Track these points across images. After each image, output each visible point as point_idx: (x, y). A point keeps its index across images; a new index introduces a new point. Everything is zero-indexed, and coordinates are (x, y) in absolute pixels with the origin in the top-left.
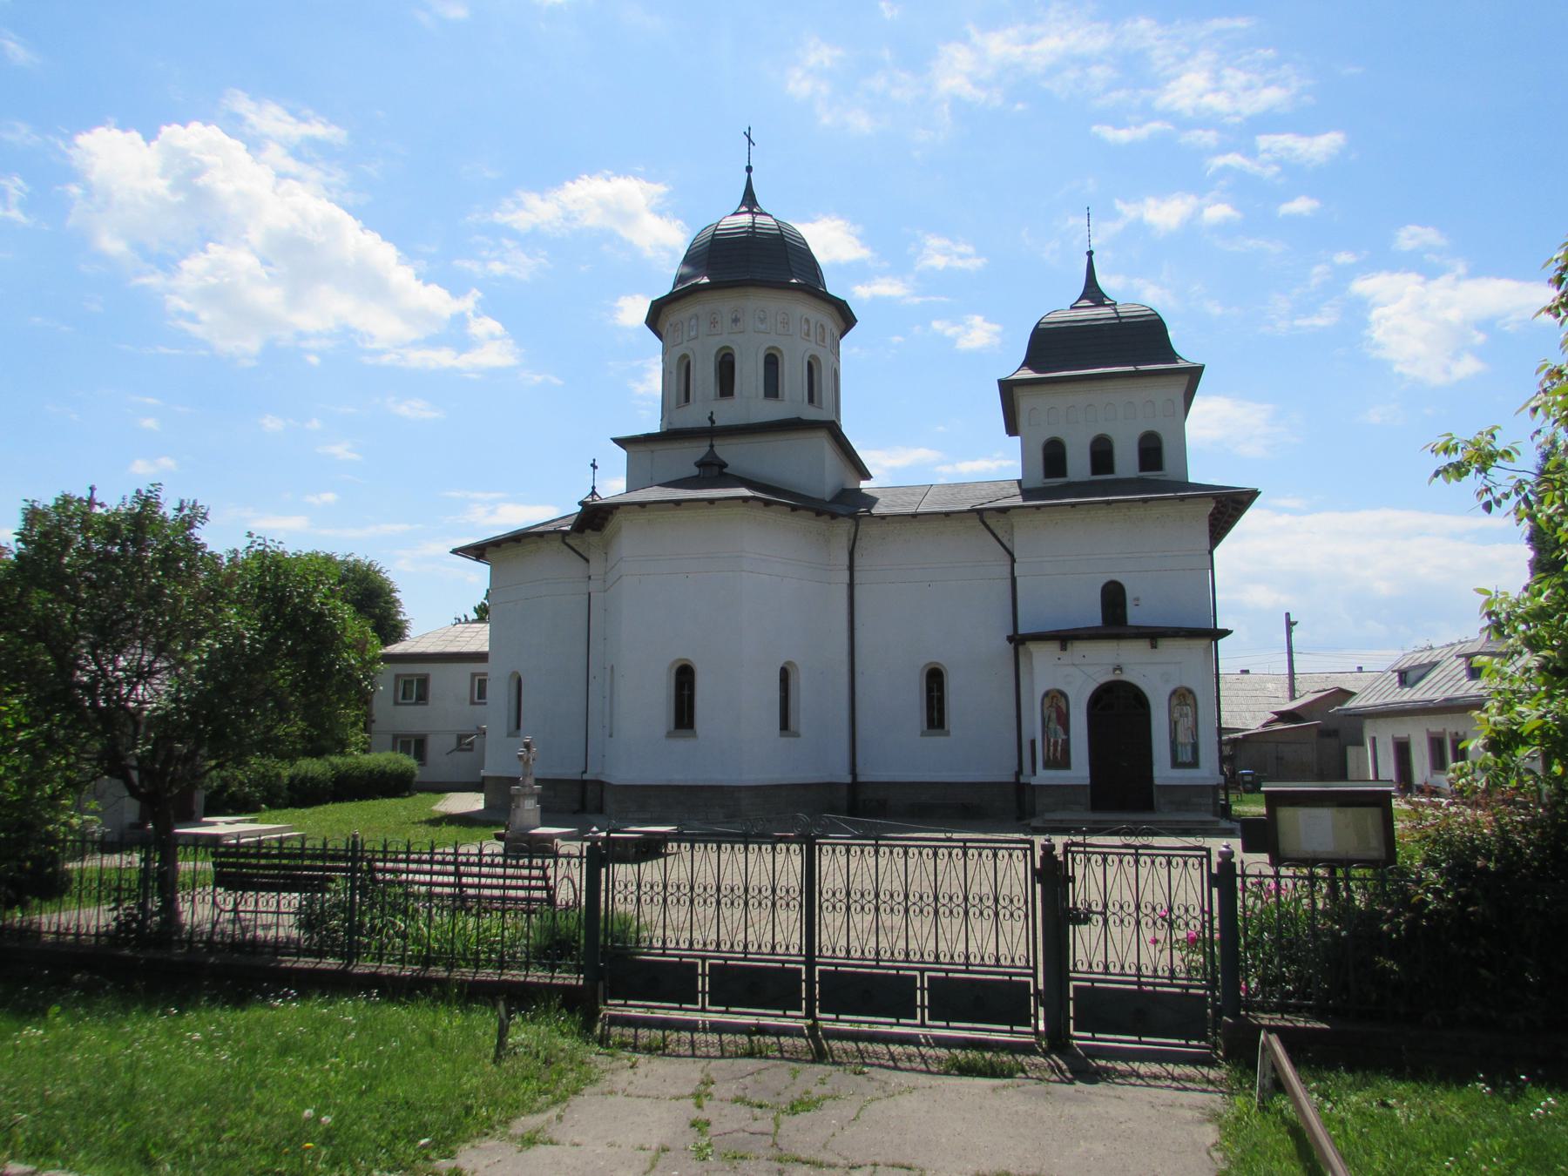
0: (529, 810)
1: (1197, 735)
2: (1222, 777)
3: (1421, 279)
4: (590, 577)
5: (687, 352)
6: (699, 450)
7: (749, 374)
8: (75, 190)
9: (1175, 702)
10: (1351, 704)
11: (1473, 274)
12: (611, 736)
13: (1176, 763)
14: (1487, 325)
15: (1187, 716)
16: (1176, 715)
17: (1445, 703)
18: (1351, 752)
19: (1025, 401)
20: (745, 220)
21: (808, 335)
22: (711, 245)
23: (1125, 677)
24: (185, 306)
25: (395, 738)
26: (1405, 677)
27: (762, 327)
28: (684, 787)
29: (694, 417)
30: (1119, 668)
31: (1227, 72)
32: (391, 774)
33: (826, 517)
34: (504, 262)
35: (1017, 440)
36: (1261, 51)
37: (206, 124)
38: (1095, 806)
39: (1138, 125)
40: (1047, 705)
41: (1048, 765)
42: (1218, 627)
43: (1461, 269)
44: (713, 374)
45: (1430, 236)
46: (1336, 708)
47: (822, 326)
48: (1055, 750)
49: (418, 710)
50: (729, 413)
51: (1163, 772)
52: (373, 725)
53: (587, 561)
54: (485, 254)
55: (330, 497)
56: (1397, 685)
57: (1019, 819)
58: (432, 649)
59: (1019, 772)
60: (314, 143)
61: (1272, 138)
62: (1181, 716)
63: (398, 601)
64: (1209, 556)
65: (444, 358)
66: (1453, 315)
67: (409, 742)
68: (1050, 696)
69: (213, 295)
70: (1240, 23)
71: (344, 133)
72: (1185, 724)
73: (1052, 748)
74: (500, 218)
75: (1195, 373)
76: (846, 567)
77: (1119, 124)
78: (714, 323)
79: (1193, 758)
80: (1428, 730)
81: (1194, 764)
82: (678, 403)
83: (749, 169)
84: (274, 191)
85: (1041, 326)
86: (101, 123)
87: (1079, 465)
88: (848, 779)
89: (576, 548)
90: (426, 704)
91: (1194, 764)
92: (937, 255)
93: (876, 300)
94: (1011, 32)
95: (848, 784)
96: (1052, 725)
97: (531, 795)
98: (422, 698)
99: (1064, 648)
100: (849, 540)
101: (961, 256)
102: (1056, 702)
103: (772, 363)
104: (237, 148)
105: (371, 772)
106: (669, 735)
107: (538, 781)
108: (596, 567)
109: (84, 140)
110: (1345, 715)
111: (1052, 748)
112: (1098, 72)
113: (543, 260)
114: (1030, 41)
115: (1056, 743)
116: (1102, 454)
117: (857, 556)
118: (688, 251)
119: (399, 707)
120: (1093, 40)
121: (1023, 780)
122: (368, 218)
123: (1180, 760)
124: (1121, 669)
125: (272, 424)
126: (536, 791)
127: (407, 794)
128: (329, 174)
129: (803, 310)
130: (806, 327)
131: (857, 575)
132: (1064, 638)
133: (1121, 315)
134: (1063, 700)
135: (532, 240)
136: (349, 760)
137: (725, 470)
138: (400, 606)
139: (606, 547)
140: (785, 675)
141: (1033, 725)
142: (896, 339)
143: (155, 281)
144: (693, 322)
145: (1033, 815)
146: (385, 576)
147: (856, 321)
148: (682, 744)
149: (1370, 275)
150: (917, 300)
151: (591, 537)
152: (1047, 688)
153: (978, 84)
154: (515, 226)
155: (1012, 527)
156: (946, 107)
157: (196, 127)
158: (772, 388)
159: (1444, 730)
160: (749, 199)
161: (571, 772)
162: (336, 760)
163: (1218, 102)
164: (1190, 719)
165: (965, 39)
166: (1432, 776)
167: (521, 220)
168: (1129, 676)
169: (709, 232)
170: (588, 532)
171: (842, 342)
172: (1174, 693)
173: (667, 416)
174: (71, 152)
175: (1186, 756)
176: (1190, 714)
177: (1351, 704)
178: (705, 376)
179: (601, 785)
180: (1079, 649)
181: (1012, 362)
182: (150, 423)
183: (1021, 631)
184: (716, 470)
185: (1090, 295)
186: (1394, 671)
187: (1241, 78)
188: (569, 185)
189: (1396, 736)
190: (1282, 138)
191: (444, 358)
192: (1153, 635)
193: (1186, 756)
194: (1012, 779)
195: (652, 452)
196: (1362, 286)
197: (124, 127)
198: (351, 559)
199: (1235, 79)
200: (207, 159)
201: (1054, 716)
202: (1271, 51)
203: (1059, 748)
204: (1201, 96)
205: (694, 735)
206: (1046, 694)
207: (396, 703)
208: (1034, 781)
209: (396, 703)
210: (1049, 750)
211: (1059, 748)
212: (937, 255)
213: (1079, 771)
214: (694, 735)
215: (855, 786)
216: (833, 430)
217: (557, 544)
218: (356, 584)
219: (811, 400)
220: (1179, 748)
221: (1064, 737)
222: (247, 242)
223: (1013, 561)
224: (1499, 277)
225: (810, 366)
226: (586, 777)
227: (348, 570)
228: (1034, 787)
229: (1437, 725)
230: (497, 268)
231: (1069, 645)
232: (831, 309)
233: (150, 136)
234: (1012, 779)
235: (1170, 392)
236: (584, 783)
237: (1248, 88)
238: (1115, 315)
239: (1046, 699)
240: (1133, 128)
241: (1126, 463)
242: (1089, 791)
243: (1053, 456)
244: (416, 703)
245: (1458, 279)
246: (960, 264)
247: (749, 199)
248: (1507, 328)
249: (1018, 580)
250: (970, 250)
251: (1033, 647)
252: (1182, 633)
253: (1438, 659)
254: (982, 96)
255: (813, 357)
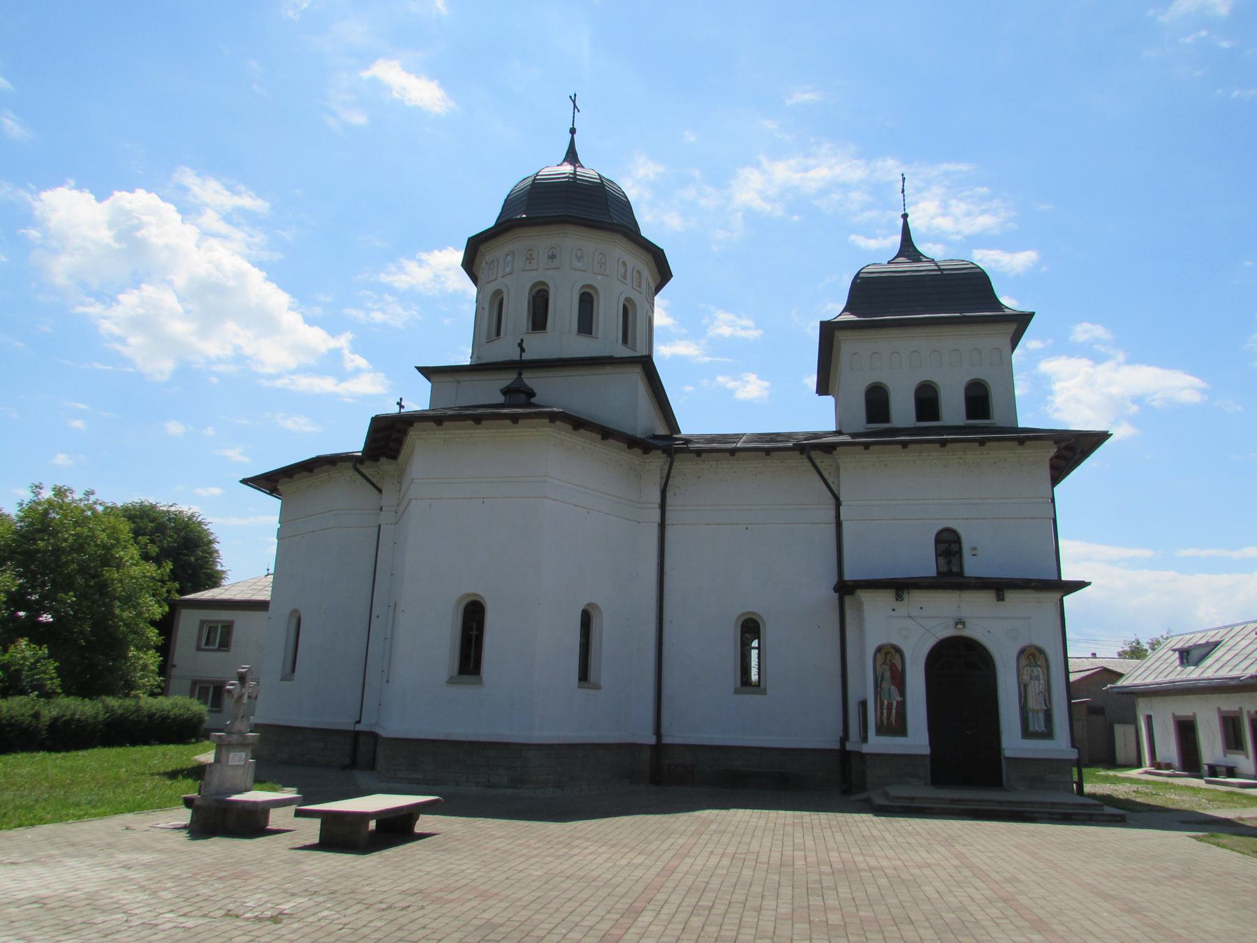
0: (233, 767)
1: (1050, 703)
2: (1076, 750)
3: (1090, 363)
4: (381, 509)
5: (501, 288)
6: (507, 379)
7: (563, 309)
8: (34, 234)
9: (1024, 662)
10: (1121, 683)
11: (1130, 361)
12: (388, 682)
13: (1027, 733)
14: (1138, 400)
15: (1037, 678)
16: (1026, 677)
17: (1250, 680)
18: (1119, 730)
19: (847, 346)
20: (568, 169)
21: (625, 277)
22: (530, 189)
23: (967, 633)
24: (117, 331)
25: (195, 683)
26: (1187, 656)
27: (579, 265)
28: (464, 742)
29: (505, 350)
30: (960, 622)
31: (953, 202)
32: (175, 720)
33: (638, 451)
34: (384, 312)
35: (829, 400)
36: (978, 189)
37: (149, 192)
38: (937, 779)
39: (885, 237)
40: (880, 661)
41: (881, 731)
42: (1063, 579)
43: (1121, 357)
44: (525, 314)
45: (1099, 331)
46: (1109, 686)
47: (639, 272)
48: (889, 713)
49: (221, 655)
50: (538, 347)
51: (1013, 742)
52: (174, 670)
53: (380, 491)
54: (369, 305)
55: (216, 491)
56: (1178, 662)
57: (846, 792)
58: (239, 597)
59: (845, 738)
60: (242, 211)
61: (986, 252)
62: (1031, 679)
63: (217, 551)
64: (1052, 504)
65: (327, 385)
66: (1114, 390)
67: (207, 689)
68: (883, 652)
69: (140, 323)
70: (963, 167)
71: (267, 205)
72: (1035, 688)
73: (885, 711)
74: (384, 278)
75: (1022, 321)
76: (657, 506)
77: (870, 235)
78: (530, 259)
79: (1046, 727)
80: (1219, 709)
81: (1048, 734)
82: (489, 336)
83: (573, 131)
84: (198, 246)
85: (861, 275)
86: (61, 183)
87: (903, 411)
88: (652, 740)
89: (370, 477)
90: (228, 651)
91: (1048, 734)
92: (725, 326)
93: (676, 359)
94: (793, 162)
95: (651, 746)
96: (885, 685)
97: (242, 745)
98: (225, 645)
99: (899, 598)
100: (662, 478)
101: (744, 328)
102: (890, 658)
103: (587, 301)
104: (169, 210)
105: (151, 716)
106: (451, 681)
107: (256, 728)
108: (388, 498)
109: (47, 196)
110: (1118, 693)
111: (885, 711)
112: (856, 196)
113: (414, 313)
114: (806, 169)
115: (890, 705)
116: (927, 401)
117: (668, 494)
118: (508, 196)
119: (202, 654)
120: (850, 170)
121: (849, 746)
122: (275, 274)
123: (1031, 729)
124: (963, 624)
125: (175, 428)
126: (249, 741)
127: (193, 740)
128: (251, 236)
129: (619, 252)
130: (623, 270)
131: (668, 514)
132: (900, 587)
133: (942, 267)
134: (898, 657)
135: (409, 297)
136: (129, 702)
137: (533, 400)
138: (219, 557)
139: (400, 476)
140: (586, 619)
141: (863, 684)
142: (689, 389)
143: (95, 310)
144: (509, 258)
145: (862, 787)
146: (206, 528)
147: (672, 276)
148: (465, 692)
149: (1052, 359)
150: (707, 359)
151: (385, 465)
152: (879, 643)
153: (765, 199)
154: (396, 285)
155: (838, 469)
156: (740, 214)
157: (141, 193)
158: (586, 325)
159: (1241, 709)
160: (571, 156)
161: (343, 721)
162: (113, 702)
163: (945, 223)
164: (1042, 682)
165: (758, 165)
166: (1225, 755)
167: (401, 281)
168: (973, 631)
169: (529, 181)
170: (383, 460)
171: (656, 298)
172: (1022, 652)
173: (476, 352)
174: (37, 204)
175: (1038, 725)
176: (1041, 677)
177: (1121, 683)
178: (517, 311)
179: (374, 736)
180: (917, 598)
181: (834, 307)
182: (78, 424)
183: (848, 576)
184: (522, 398)
185: (906, 253)
186: (1174, 650)
187: (963, 207)
188: (436, 252)
189: (1179, 713)
190: (992, 252)
191: (327, 385)
192: (999, 587)
193: (1038, 725)
194: (837, 746)
195: (458, 382)
196: (1046, 366)
197: (80, 187)
198: (173, 509)
199: (959, 207)
200: (144, 218)
201: (887, 675)
202: (985, 189)
203: (894, 711)
204: (933, 218)
205: (480, 682)
206: (879, 650)
207: (199, 649)
208: (865, 749)
209: (199, 649)
210: (882, 713)
211: (894, 711)
212: (725, 326)
213: (917, 739)
214: (480, 682)
215: (659, 748)
216: (646, 365)
217: (348, 472)
218: (175, 533)
219: (625, 340)
220: (1030, 714)
221: (899, 699)
222: (171, 284)
223: (838, 504)
224: (1149, 365)
225: (625, 309)
226: (359, 728)
227: (170, 519)
228: (862, 756)
229: (1230, 704)
230: (378, 317)
231: (905, 595)
232: (650, 258)
233: (101, 196)
234: (837, 746)
235: (998, 336)
236: (357, 734)
237: (968, 214)
238: (936, 268)
239: (879, 656)
240: (880, 239)
241: (953, 410)
242: (928, 761)
243: (877, 402)
244: (218, 650)
245: (1118, 364)
246: (743, 334)
247: (571, 156)
248: (1153, 403)
249: (844, 523)
250: (751, 323)
251: (865, 596)
252: (1033, 584)
253: (1217, 639)
254: (767, 207)
255: (628, 300)
